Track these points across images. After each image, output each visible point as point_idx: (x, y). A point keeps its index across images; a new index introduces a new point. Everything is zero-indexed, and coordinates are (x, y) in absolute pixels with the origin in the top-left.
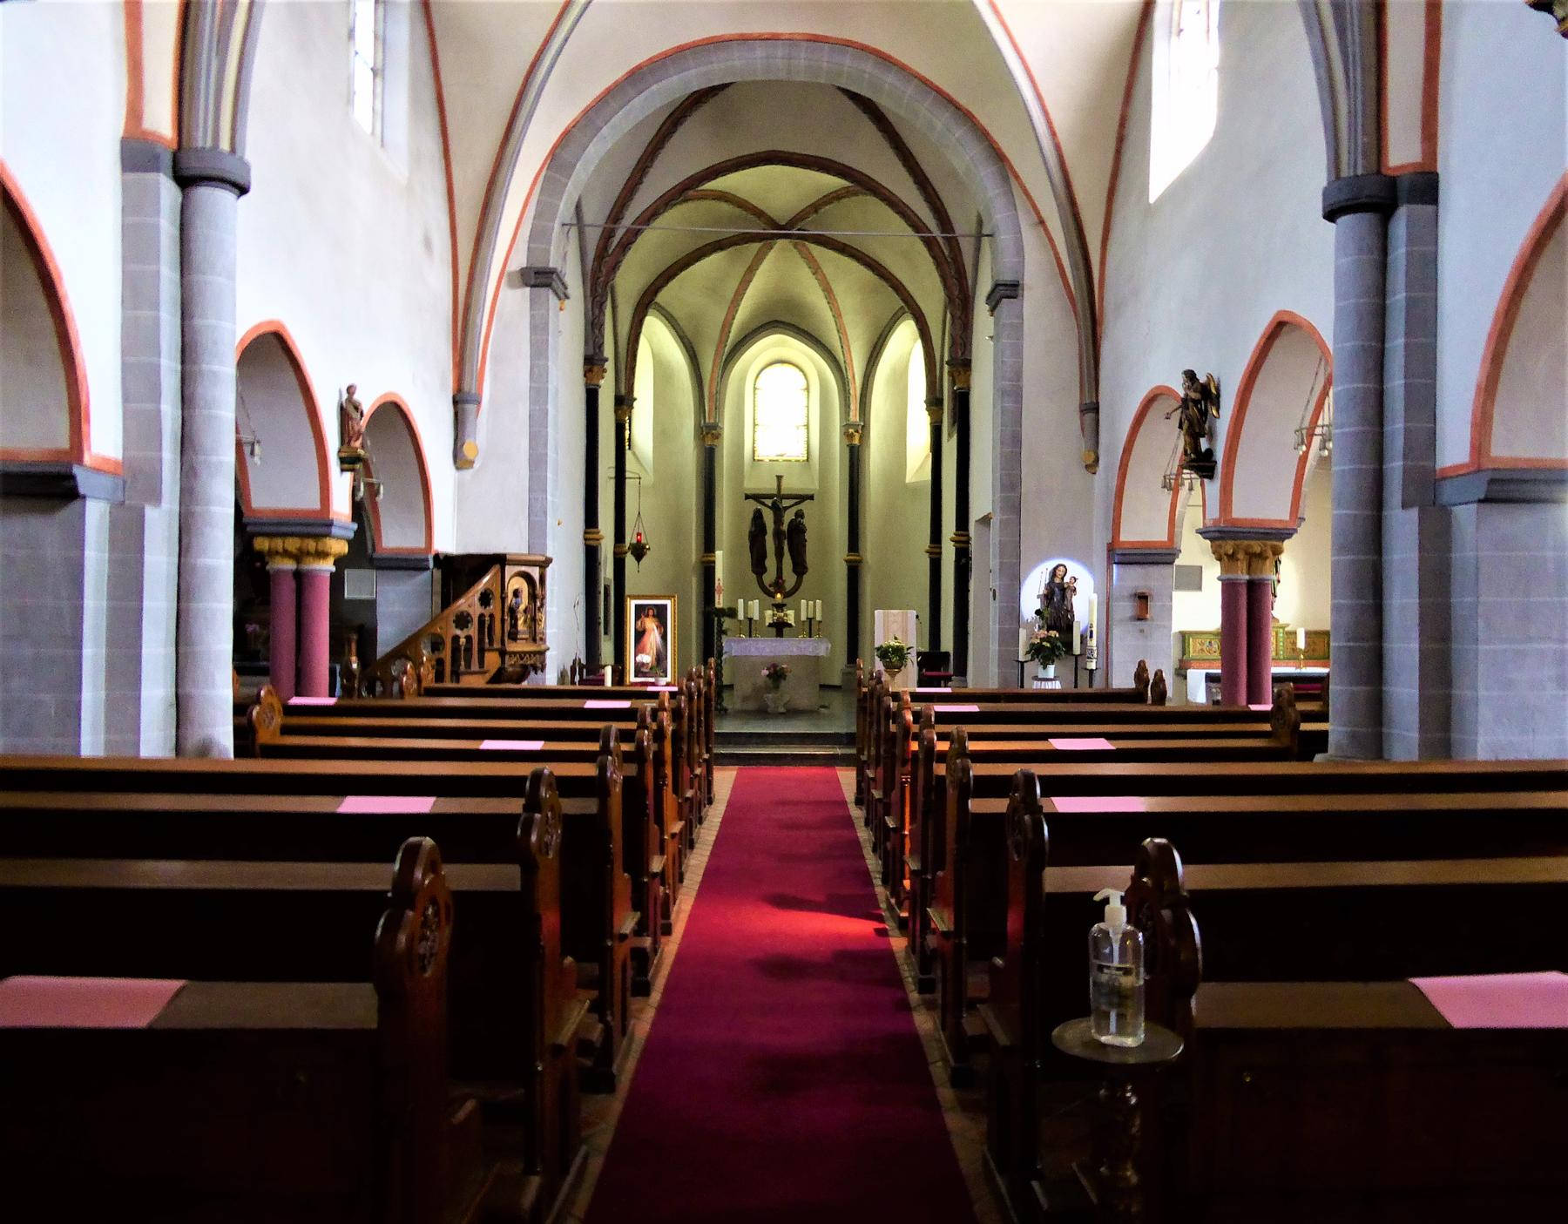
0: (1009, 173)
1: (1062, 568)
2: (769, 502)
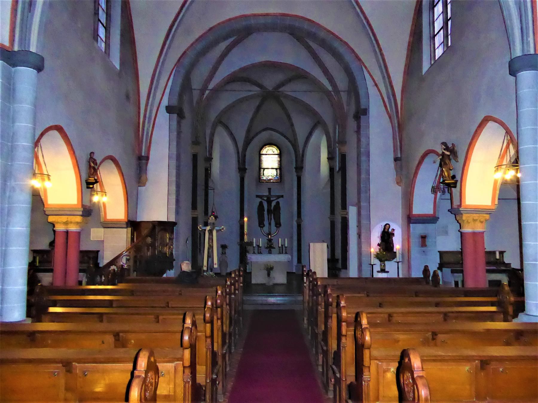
0: (364, 68)
1: (388, 225)
2: (265, 199)
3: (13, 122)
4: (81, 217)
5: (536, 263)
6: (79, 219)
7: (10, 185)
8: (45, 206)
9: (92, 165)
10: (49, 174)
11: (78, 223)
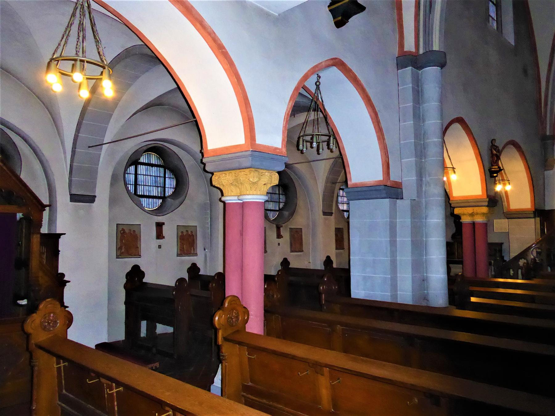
3: (424, 121)
4: (487, 207)
5: (113, 391)
6: (485, 210)
7: (425, 180)
8: (451, 199)
9: (495, 152)
10: (454, 167)
11: (483, 214)
